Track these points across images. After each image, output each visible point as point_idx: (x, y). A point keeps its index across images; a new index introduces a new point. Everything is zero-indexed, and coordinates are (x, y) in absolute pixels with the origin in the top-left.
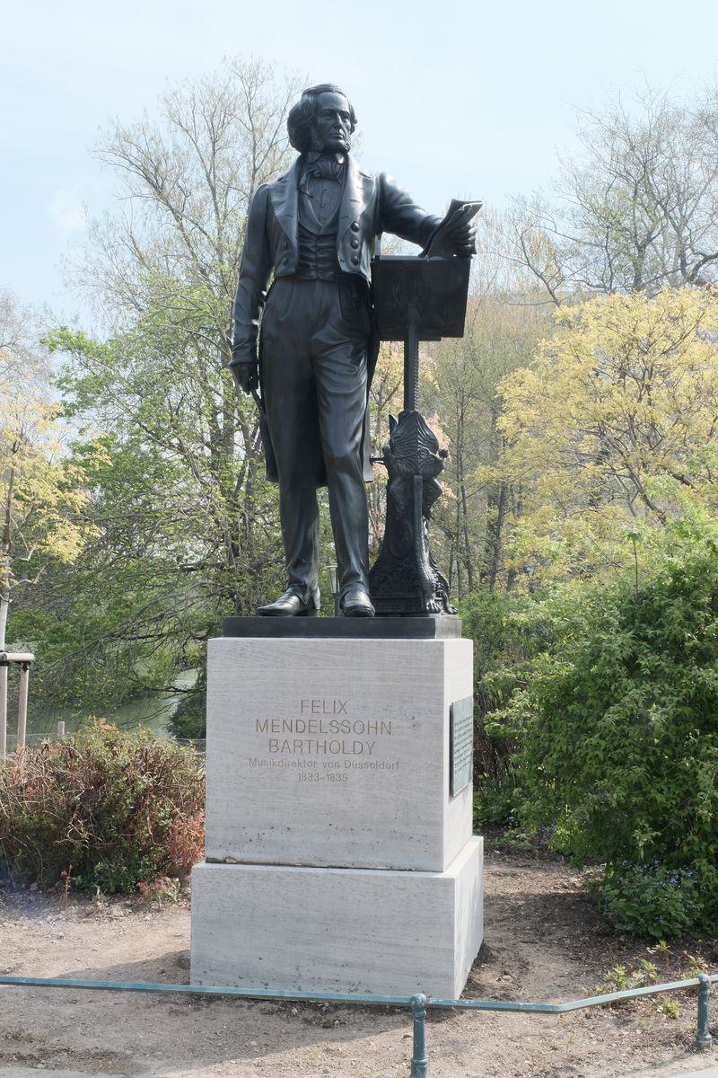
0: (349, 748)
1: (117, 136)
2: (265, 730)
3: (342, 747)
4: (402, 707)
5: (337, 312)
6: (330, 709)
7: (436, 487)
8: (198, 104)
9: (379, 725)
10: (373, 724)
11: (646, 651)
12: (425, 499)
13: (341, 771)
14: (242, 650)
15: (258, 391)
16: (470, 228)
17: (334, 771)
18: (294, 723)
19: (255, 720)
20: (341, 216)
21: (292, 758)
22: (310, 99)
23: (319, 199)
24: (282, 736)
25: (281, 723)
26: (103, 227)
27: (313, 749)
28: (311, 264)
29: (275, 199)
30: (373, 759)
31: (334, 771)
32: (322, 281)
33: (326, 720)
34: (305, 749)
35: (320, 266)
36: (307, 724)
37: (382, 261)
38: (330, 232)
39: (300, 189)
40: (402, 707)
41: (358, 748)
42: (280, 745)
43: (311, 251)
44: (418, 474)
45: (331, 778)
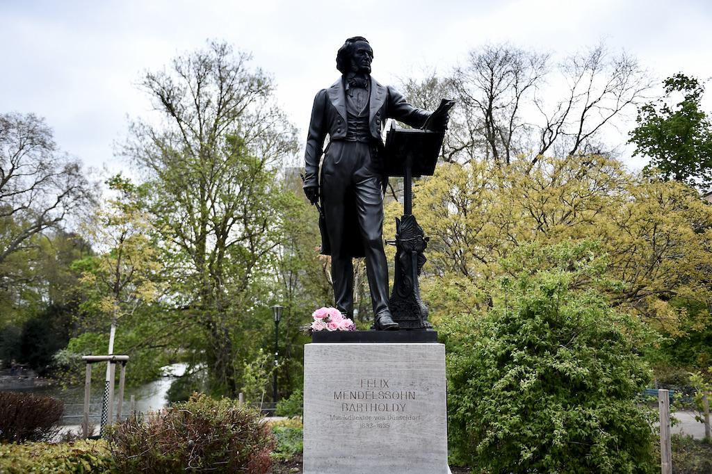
0: (390, 407)
1: (148, 77)
4: (421, 383)
5: (368, 158)
7: (424, 257)
8: (192, 64)
9: (408, 394)
11: (515, 349)
14: (325, 350)
15: (319, 203)
17: (381, 422)
18: (357, 393)
21: (356, 414)
23: (356, 98)
26: (137, 125)
27: (369, 409)
29: (331, 97)
30: (404, 414)
31: (381, 422)
34: (364, 409)
35: (358, 133)
38: (364, 115)
39: (346, 93)
40: (421, 383)
41: (396, 407)
44: (414, 250)
45: (379, 426)
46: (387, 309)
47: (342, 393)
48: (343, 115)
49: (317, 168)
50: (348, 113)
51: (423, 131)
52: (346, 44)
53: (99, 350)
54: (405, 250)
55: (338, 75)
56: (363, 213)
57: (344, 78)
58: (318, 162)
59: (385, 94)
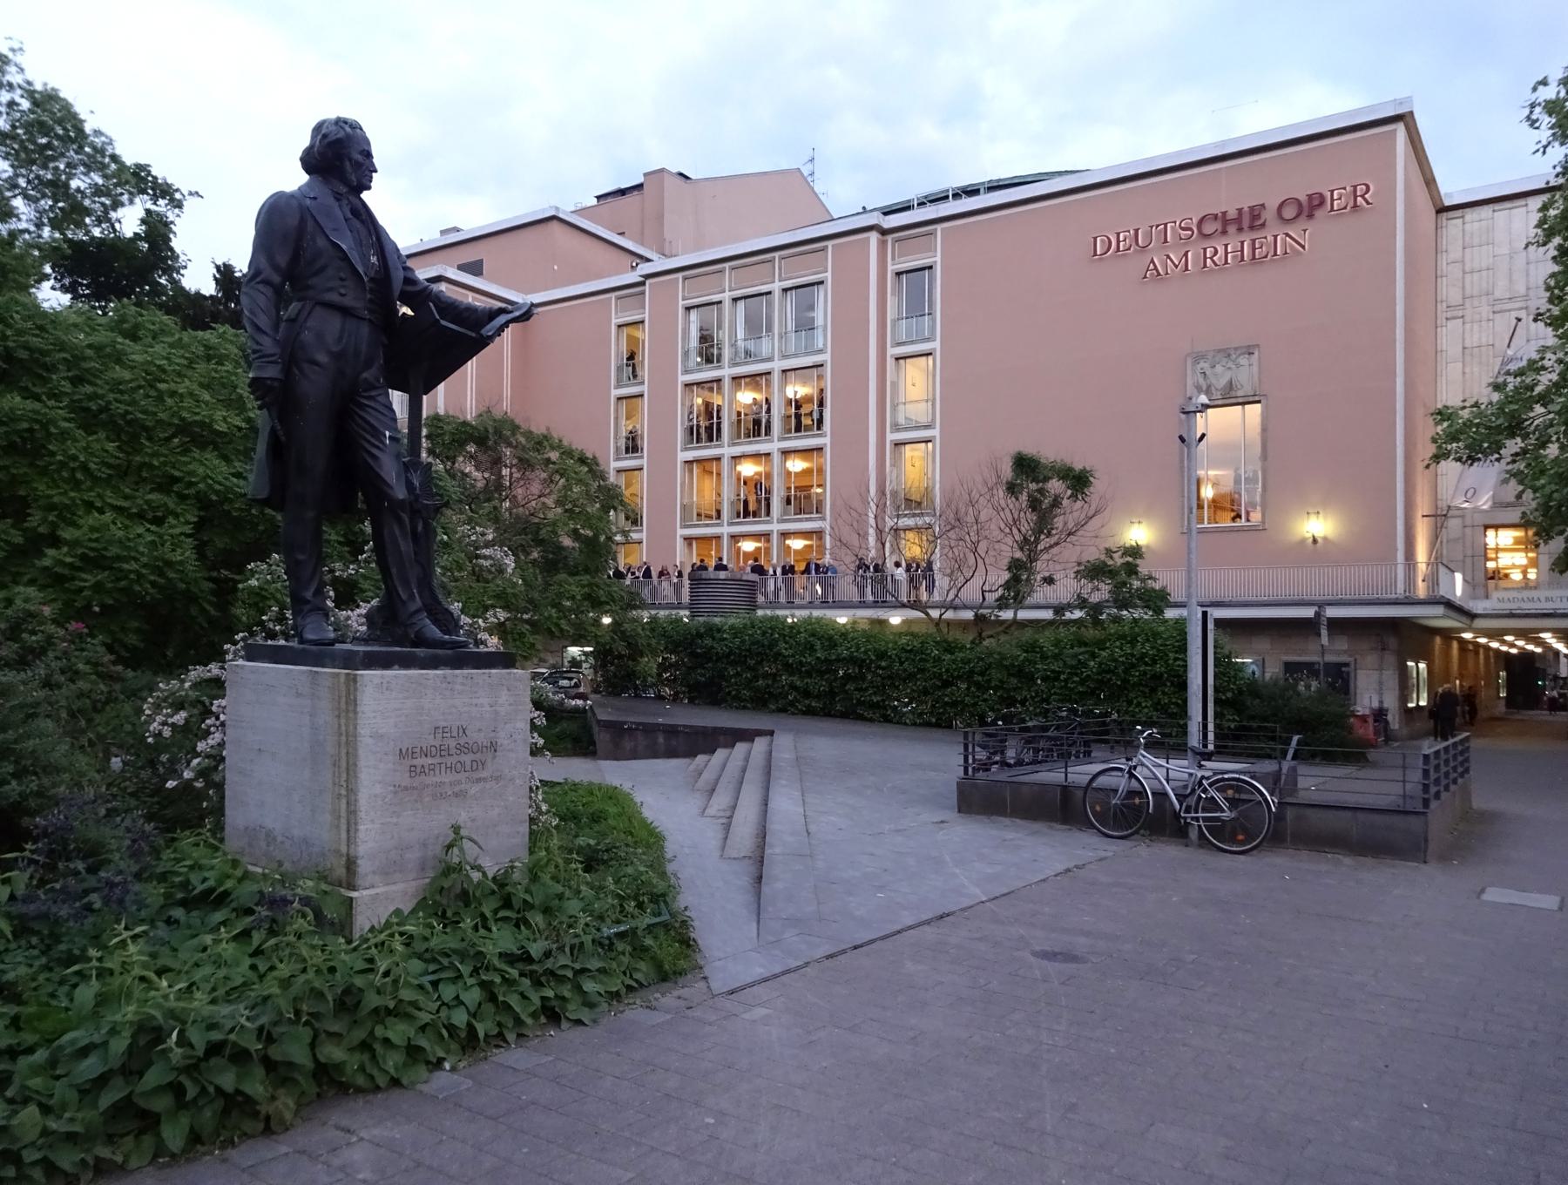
6: (455, 734)
17: (457, 789)
24: (419, 762)
25: (418, 750)
42: (418, 770)
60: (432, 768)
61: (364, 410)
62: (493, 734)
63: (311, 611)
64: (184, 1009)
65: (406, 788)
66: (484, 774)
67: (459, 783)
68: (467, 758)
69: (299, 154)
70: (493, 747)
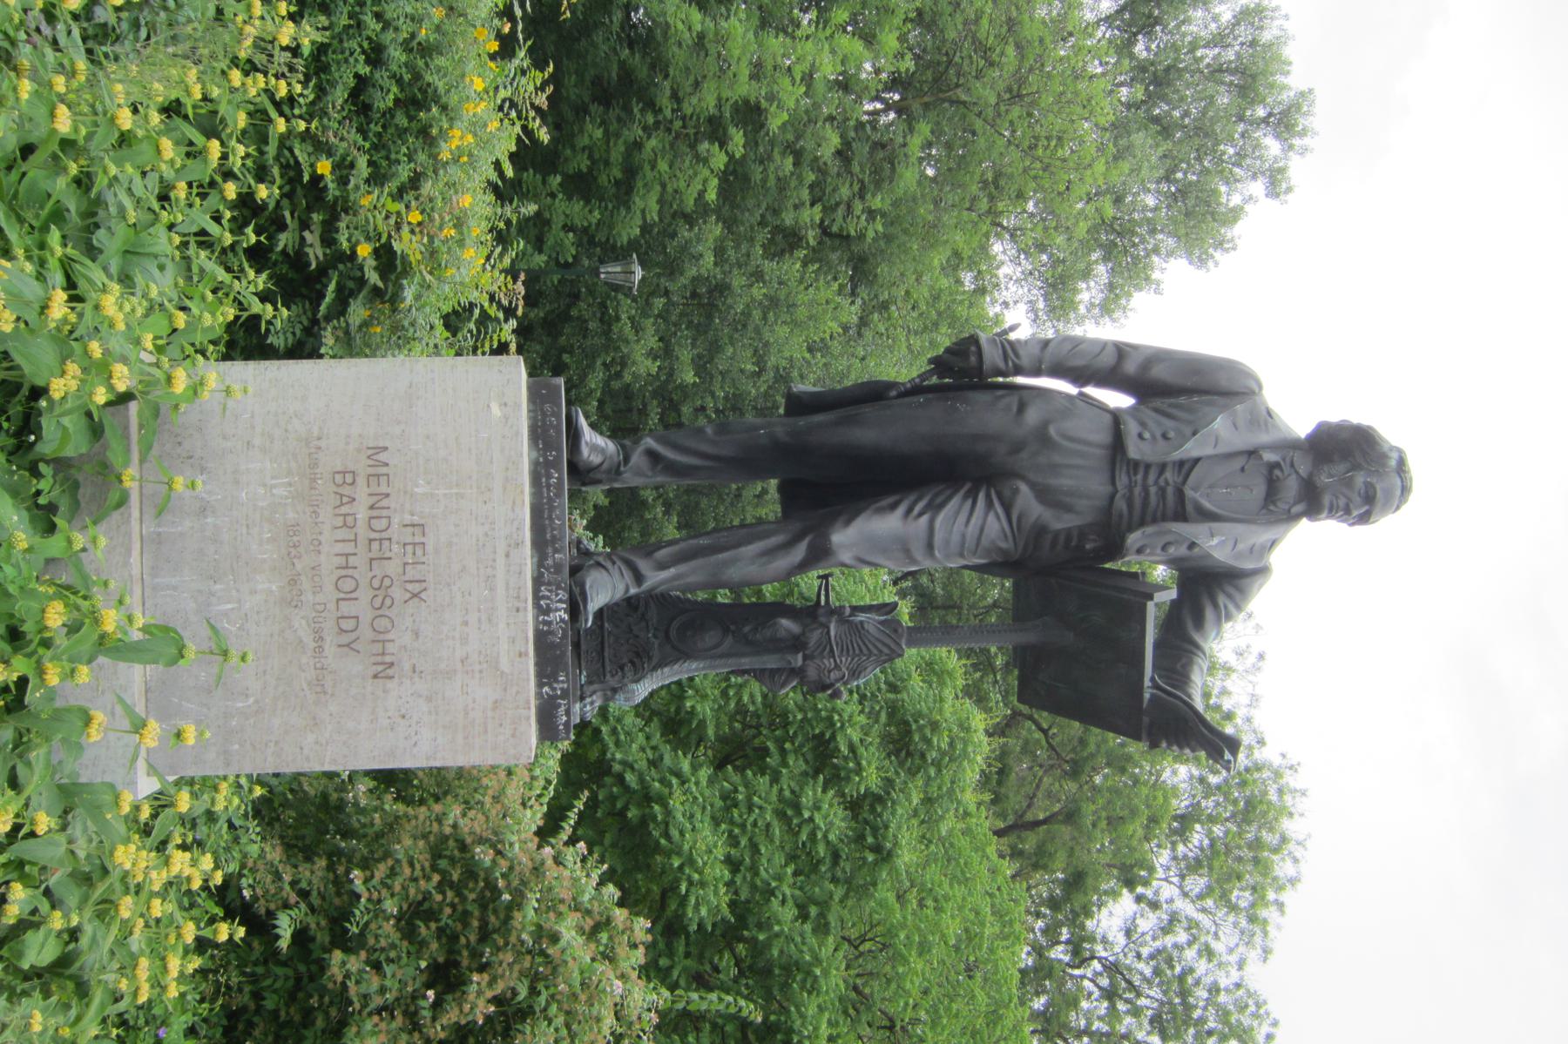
0: (346, 608)
2: (372, 463)
3: (349, 596)
5: (1060, 522)
6: (411, 573)
9: (388, 659)
10: (390, 648)
12: (763, 671)
13: (308, 597)
15: (934, 380)
16: (1193, 751)
17: (306, 584)
18: (385, 513)
19: (387, 444)
20: (1215, 525)
21: (326, 513)
22: (1393, 463)
24: (362, 493)
25: (384, 489)
27: (340, 548)
28: (1139, 477)
32: (1112, 497)
33: (393, 568)
36: (384, 535)
37: (1145, 605)
38: (1189, 508)
42: (346, 490)
43: (1159, 477)
44: (805, 658)
46: (633, 591)
47: (384, 470)
48: (1191, 449)
49: (1037, 373)
50: (1197, 461)
51: (1147, 683)
52: (1392, 448)
53: (596, 856)
54: (803, 633)
55: (1300, 425)
56: (931, 501)
57: (1293, 445)
58: (1057, 371)
59: (1248, 565)
60: (348, 523)
61: (965, 497)
62: (407, 666)
63: (591, 566)
64: (567, 664)
65: (314, 465)
66: (330, 649)
67: (318, 589)
68: (362, 607)
69: (1334, 417)
70: (384, 670)
